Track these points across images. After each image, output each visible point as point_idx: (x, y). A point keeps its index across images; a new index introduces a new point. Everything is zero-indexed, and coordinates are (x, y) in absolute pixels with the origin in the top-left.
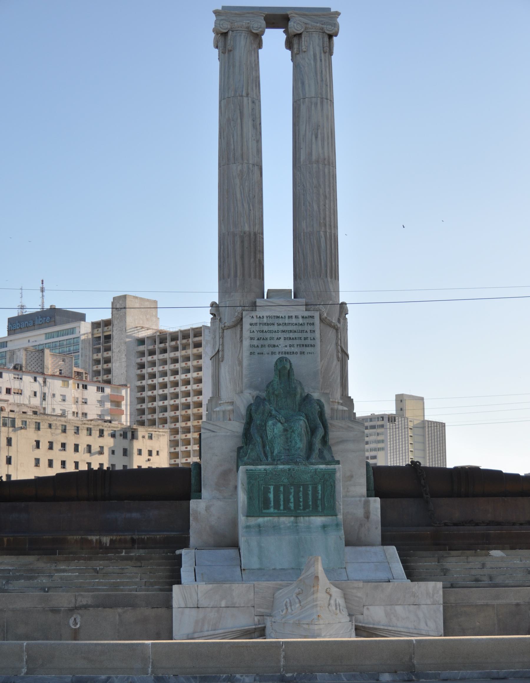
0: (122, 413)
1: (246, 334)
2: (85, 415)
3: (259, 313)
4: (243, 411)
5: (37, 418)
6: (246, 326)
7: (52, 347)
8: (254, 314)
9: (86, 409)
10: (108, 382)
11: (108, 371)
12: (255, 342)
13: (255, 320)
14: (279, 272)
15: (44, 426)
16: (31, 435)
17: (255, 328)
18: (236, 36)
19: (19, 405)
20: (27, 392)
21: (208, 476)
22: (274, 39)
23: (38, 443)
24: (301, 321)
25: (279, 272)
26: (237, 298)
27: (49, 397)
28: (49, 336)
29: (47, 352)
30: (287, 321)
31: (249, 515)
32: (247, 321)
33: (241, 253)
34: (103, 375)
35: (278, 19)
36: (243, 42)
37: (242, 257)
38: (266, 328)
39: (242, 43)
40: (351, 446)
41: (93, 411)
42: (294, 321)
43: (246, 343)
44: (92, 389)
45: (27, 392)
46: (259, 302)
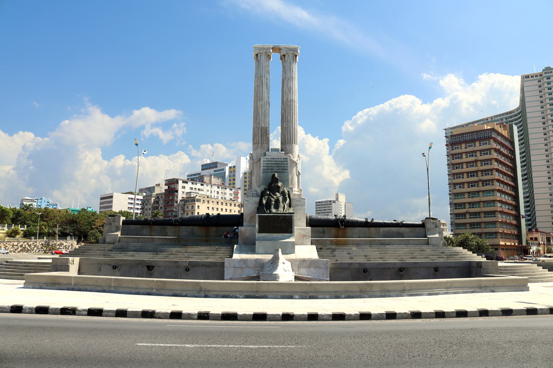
0: (238, 198)
1: (262, 165)
2: (225, 198)
3: (267, 157)
4: (260, 194)
5: (208, 199)
6: (262, 162)
7: (215, 175)
8: (265, 157)
9: (226, 196)
10: (234, 187)
11: (234, 184)
12: (265, 168)
13: (265, 160)
14: (275, 143)
15: (211, 202)
16: (206, 205)
17: (265, 162)
18: (262, 56)
19: (202, 195)
20: (205, 190)
21: (246, 218)
22: (275, 57)
23: (208, 208)
24: (282, 160)
25: (275, 143)
26: (259, 151)
27: (213, 192)
28: (215, 171)
29: (212, 176)
30: (277, 160)
31: (259, 232)
32: (262, 160)
33: (261, 136)
34: (232, 185)
35: (276, 49)
36: (264, 57)
37: (261, 136)
38: (269, 163)
39: (263, 58)
40: (299, 207)
41: (228, 197)
42: (280, 160)
43: (262, 168)
44: (228, 190)
45: (205, 190)
46: (267, 153)
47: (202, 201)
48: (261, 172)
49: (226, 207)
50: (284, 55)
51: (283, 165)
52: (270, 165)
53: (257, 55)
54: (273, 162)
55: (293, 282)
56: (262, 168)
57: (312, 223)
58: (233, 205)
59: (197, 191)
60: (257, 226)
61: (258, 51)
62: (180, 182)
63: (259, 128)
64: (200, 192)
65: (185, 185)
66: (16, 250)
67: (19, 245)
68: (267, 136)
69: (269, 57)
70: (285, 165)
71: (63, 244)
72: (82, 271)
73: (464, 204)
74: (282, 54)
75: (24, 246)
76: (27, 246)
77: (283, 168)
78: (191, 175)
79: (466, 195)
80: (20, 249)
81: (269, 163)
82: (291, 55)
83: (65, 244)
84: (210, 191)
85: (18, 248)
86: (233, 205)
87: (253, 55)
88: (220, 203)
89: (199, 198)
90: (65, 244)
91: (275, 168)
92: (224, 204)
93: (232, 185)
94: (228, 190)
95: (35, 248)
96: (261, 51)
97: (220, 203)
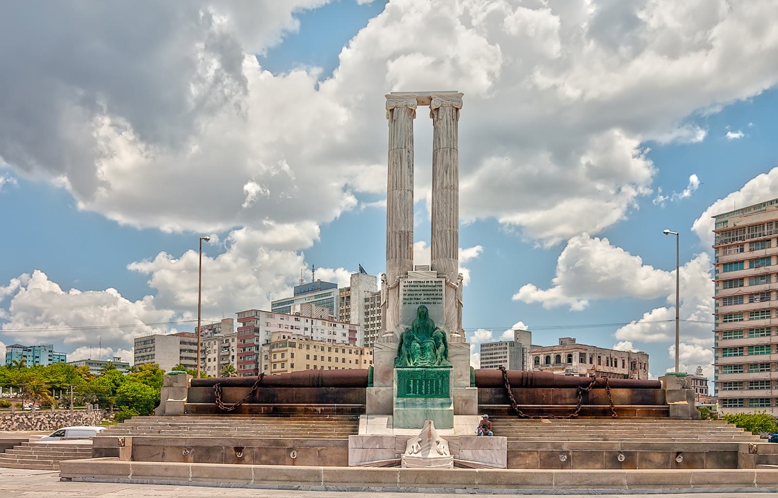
1: (401, 292)
4: (399, 337)
6: (401, 287)
8: (406, 280)
9: (335, 337)
11: (348, 316)
12: (407, 297)
13: (407, 284)
14: (422, 252)
15: (312, 347)
16: (304, 351)
17: (406, 288)
24: (434, 284)
25: (422, 252)
31: (398, 397)
32: (402, 284)
35: (425, 100)
38: (413, 288)
39: (402, 116)
42: (430, 284)
47: (297, 345)
48: (401, 303)
49: (337, 355)
50: (437, 109)
51: (435, 292)
52: (414, 293)
53: (392, 110)
54: (419, 288)
55: (452, 469)
56: (401, 297)
57: (479, 381)
58: (347, 351)
59: (290, 330)
60: (395, 386)
61: (393, 104)
62: (262, 317)
63: (396, 233)
64: (295, 331)
65: (270, 320)
66: (9, 426)
67: (13, 419)
68: (410, 246)
69: (412, 113)
70: (439, 292)
71: (81, 417)
72: (135, 458)
73: (742, 279)
74: (434, 107)
75: (21, 420)
76: (25, 420)
77: (435, 297)
78: (279, 304)
79: (746, 265)
80: (16, 424)
81: (413, 288)
82: (448, 109)
83: (85, 416)
84: (310, 330)
85: (12, 424)
86: (347, 351)
87: (385, 112)
88: (326, 349)
89: (294, 341)
90: (85, 416)
91: (422, 296)
92: (333, 350)
93: (345, 318)
94: (339, 326)
95: (39, 423)
96: (399, 104)
97: (326, 349)
